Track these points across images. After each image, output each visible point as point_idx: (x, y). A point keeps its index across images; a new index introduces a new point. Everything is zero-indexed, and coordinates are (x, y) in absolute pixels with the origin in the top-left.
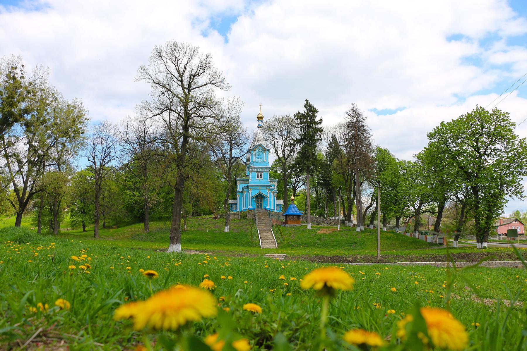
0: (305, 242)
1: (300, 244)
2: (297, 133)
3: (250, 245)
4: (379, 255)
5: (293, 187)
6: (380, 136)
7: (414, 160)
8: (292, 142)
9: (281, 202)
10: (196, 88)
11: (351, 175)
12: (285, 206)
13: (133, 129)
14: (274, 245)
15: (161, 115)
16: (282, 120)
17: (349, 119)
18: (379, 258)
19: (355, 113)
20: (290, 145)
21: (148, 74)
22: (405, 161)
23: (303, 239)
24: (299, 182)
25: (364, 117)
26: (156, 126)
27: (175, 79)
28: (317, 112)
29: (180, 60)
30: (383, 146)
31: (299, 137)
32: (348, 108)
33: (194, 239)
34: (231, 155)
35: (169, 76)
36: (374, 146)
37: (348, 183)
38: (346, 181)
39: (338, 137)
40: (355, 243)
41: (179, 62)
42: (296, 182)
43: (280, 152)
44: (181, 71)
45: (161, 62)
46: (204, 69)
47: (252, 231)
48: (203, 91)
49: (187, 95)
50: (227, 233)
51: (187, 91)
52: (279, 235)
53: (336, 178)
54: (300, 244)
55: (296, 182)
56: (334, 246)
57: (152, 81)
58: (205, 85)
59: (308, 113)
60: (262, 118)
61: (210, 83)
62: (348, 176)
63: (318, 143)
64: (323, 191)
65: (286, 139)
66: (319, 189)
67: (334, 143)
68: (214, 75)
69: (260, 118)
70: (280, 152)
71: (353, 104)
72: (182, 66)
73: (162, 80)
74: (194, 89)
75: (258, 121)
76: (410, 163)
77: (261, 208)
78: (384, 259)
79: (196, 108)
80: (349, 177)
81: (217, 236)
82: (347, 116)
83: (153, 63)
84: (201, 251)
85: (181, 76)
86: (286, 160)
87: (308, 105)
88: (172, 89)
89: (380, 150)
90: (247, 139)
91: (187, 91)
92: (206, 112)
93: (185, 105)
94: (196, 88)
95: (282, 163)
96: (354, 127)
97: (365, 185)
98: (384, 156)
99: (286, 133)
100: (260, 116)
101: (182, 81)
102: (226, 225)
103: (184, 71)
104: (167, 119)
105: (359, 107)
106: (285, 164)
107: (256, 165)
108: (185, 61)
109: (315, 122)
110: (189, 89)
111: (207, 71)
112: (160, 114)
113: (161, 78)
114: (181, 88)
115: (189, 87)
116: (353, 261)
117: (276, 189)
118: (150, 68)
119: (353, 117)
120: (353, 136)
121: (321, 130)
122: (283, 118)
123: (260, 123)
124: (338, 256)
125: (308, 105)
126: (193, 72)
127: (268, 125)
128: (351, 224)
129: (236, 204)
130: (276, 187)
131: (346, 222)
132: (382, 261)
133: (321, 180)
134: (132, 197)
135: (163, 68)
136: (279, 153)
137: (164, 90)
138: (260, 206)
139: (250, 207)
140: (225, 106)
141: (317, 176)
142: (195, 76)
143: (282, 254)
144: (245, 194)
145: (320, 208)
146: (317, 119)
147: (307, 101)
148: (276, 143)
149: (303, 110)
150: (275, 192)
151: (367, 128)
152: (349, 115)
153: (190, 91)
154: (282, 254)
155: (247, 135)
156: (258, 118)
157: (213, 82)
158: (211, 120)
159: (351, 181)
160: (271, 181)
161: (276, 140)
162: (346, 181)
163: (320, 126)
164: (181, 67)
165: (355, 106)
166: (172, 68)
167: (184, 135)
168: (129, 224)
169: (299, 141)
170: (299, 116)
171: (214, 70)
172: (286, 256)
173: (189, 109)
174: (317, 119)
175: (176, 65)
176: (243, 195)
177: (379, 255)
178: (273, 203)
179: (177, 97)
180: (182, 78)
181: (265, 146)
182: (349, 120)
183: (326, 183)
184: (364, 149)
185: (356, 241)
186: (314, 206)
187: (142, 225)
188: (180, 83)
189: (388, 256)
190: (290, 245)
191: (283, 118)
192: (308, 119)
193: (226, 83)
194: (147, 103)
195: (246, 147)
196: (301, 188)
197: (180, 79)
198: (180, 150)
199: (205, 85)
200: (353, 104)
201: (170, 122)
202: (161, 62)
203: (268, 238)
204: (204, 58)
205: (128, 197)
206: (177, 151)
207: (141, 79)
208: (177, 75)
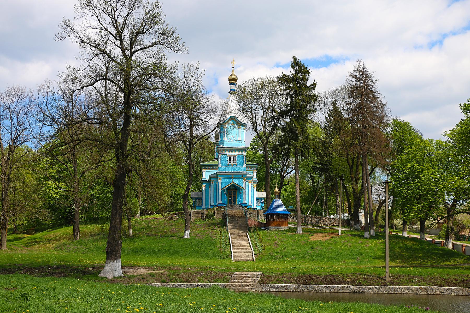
0: (293, 252)
1: (286, 256)
2: (282, 102)
3: (218, 256)
4: (388, 275)
5: (281, 173)
6: (397, 107)
7: (445, 139)
8: (275, 114)
9: (263, 194)
10: (141, 49)
11: (358, 158)
12: (268, 202)
13: (55, 104)
14: (251, 257)
15: (95, 85)
16: (261, 84)
17: (353, 82)
18: (388, 279)
19: (362, 75)
20: (274, 118)
21: (73, 30)
22: (433, 140)
23: (290, 248)
24: (288, 166)
25: (374, 79)
26: (86, 96)
27: (111, 37)
28: (308, 72)
29: (118, 11)
30: (404, 118)
31: (284, 109)
32: (351, 67)
33: (142, 249)
34: (191, 133)
35: (104, 32)
36: (389, 120)
37: (354, 169)
38: (351, 167)
39: (341, 105)
40: (361, 254)
41: (117, 14)
42: (284, 166)
43: (259, 128)
44: (120, 27)
45: (91, 14)
46: (151, 25)
47: (221, 236)
48: (150, 52)
49: (128, 59)
50: (187, 239)
51: (128, 53)
52: (257, 242)
53: (338, 161)
54: (286, 256)
55: (284, 166)
56: (331, 259)
57: (79, 40)
58: (152, 46)
59: (296, 75)
60: (235, 80)
61: (159, 42)
62: (353, 160)
63: (310, 116)
64: (321, 180)
65: (267, 110)
66: (316, 176)
67: (335, 113)
68: (165, 33)
69: (233, 81)
70: (259, 128)
71: (359, 62)
72: (120, 20)
73: (94, 37)
74: (137, 51)
75: (230, 84)
76: (439, 143)
77: (235, 203)
78: (395, 281)
79: (141, 76)
80: (355, 160)
81: (174, 243)
82: (350, 78)
83: (80, 15)
84: (149, 269)
85: (120, 33)
86: (267, 138)
87: (296, 64)
88: (108, 49)
89: (397, 125)
90: (214, 111)
91: (128, 53)
92: (156, 81)
93: (126, 75)
94: (141, 49)
95: (263, 142)
96: (361, 93)
97: (378, 172)
98: (404, 132)
99: (267, 101)
100: (233, 77)
101: (121, 40)
102: (186, 229)
103: (124, 24)
104: (102, 90)
105: (367, 66)
106: (267, 143)
107: (227, 145)
108: (124, 12)
109: (306, 87)
110: (131, 51)
111: (155, 28)
112: (92, 85)
113: (93, 35)
114: (120, 50)
115: (131, 47)
116: (352, 283)
117: (255, 177)
118: (76, 23)
119: (359, 80)
120: (359, 106)
121: (314, 98)
122: (262, 81)
123: (233, 87)
124: (331, 275)
125: (296, 64)
126: (136, 28)
127: (243, 90)
128: (358, 226)
129: (201, 198)
130: (255, 174)
131: (352, 223)
132: (392, 283)
133: (318, 164)
134: (56, 191)
135: (94, 22)
136: (258, 128)
137: (97, 52)
138: (233, 201)
139: (220, 202)
140: (179, 75)
141: (312, 159)
142: (138, 33)
143: (257, 273)
144: (212, 184)
145: (315, 204)
146: (309, 84)
147: (295, 58)
148: (254, 115)
149: (289, 72)
150: (254, 182)
151: (379, 96)
152: (354, 77)
153: (132, 53)
154: (257, 273)
155: (214, 106)
156: (230, 80)
157: (163, 41)
158: (160, 93)
159: (357, 167)
160: (248, 166)
161: (253, 112)
162: (351, 167)
163: (314, 92)
164: (118, 21)
165: (362, 64)
166: (107, 21)
167: (126, 113)
168: (54, 227)
169: (283, 114)
170: (284, 79)
171: (164, 25)
172: (263, 274)
173: (131, 79)
174: (309, 84)
175: (113, 17)
176: (210, 186)
177: (388, 275)
178: (252, 196)
179: (114, 61)
180: (120, 36)
181: (239, 119)
182: (353, 84)
183: (323, 169)
184: (374, 123)
185: (362, 251)
186: (307, 200)
187: (70, 230)
188: (118, 43)
189: (401, 276)
190: (271, 257)
191: (262, 81)
192: (297, 82)
193: (180, 43)
194: (74, 69)
195: (213, 121)
196: (290, 174)
197: (118, 37)
198: (121, 133)
199: (152, 46)
200: (359, 62)
201: (106, 95)
202: (91, 14)
203: (242, 246)
204: (150, 7)
205: (49, 190)
206: (117, 135)
207: (65, 37)
208: (114, 31)
